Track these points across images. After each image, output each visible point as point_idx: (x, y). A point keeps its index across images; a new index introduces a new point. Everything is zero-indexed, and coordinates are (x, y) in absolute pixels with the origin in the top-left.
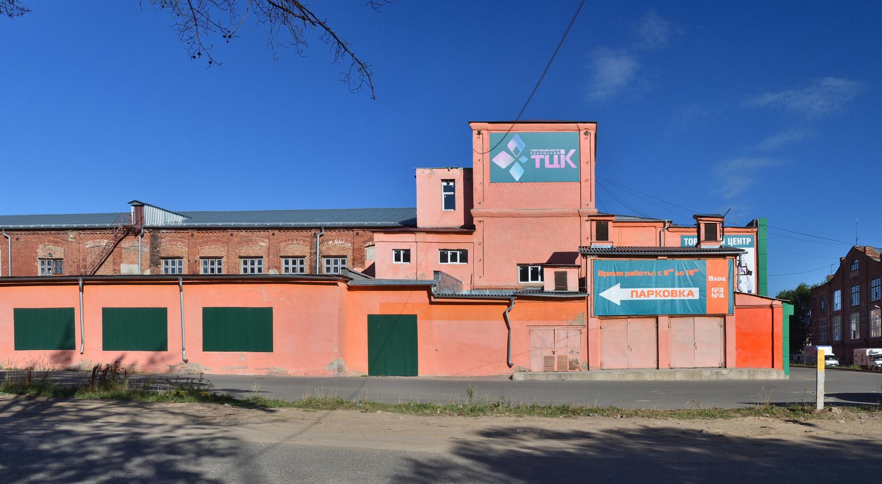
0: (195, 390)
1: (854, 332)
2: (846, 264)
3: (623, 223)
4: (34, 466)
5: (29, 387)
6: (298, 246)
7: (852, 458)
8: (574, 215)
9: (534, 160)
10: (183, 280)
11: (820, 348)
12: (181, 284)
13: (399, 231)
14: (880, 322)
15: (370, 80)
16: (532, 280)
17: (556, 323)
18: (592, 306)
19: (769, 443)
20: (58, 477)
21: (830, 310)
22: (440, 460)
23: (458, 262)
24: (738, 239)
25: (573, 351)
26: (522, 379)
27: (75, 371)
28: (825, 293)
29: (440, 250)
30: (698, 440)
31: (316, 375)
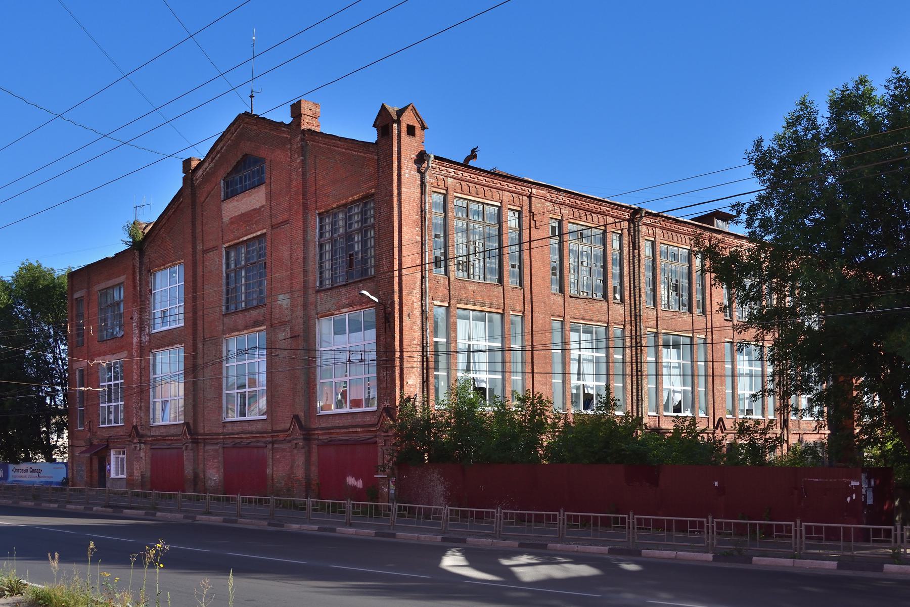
0: (800, 322)
1: (269, 525)
4: (657, 553)
6: (527, 338)
11: (112, 476)
14: (182, 393)
16: (891, 538)
17: (162, 349)
18: (239, 407)
21: (141, 329)
26: (265, 398)
28: (122, 278)
30: (578, 560)
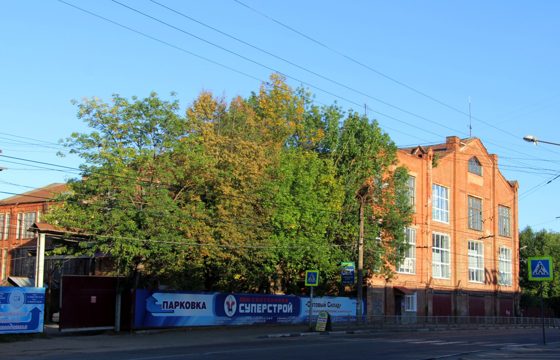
2: (71, 150)
3: (424, 192)
5: (233, 274)
7: (447, 287)
8: (422, 281)
9: (63, 276)
10: (470, 280)
12: (433, 248)
13: (522, 346)
15: (422, 237)
19: (535, 343)
20: (3, 263)
22: (31, 339)
23: (508, 248)
24: (246, 305)
25: (214, 152)
27: (427, 186)
29: (24, 304)
31: (18, 343)
